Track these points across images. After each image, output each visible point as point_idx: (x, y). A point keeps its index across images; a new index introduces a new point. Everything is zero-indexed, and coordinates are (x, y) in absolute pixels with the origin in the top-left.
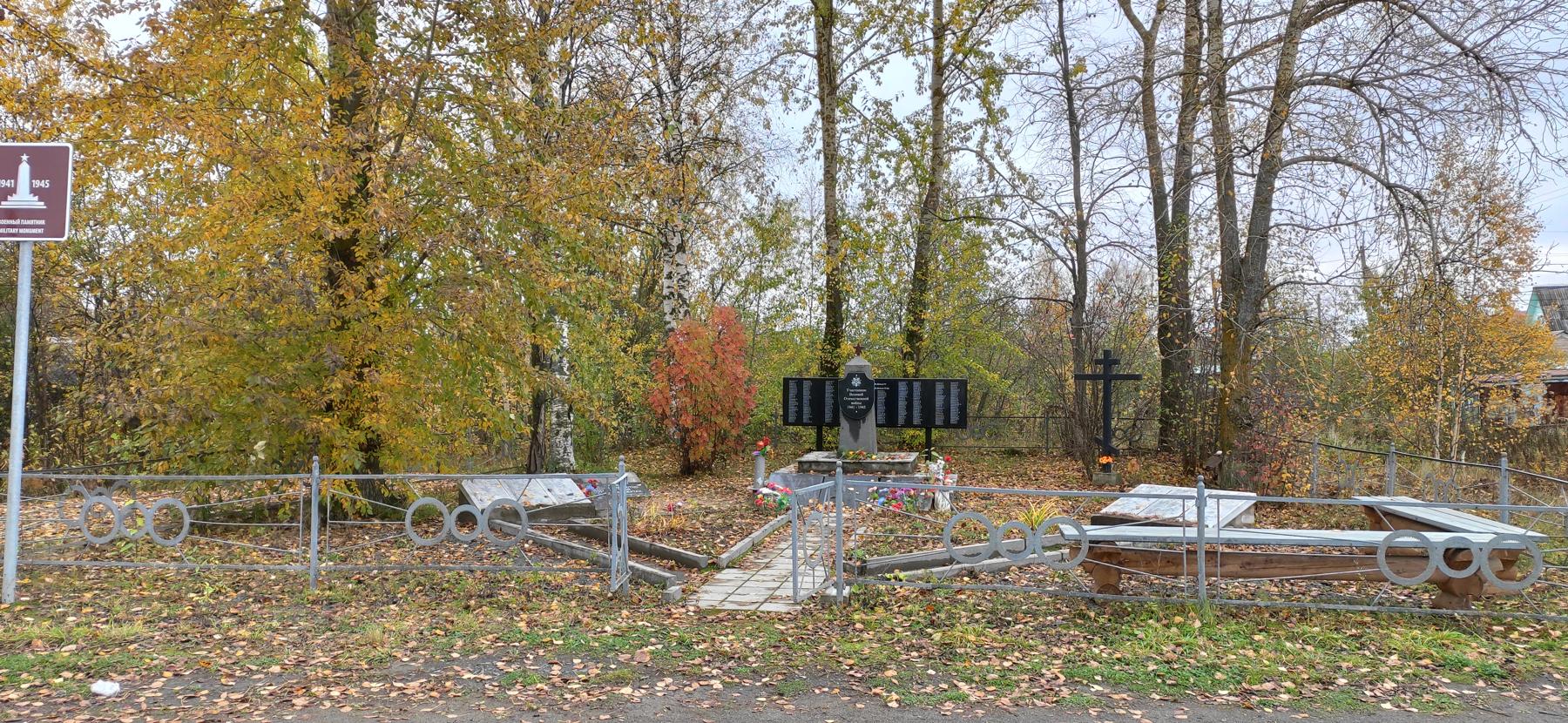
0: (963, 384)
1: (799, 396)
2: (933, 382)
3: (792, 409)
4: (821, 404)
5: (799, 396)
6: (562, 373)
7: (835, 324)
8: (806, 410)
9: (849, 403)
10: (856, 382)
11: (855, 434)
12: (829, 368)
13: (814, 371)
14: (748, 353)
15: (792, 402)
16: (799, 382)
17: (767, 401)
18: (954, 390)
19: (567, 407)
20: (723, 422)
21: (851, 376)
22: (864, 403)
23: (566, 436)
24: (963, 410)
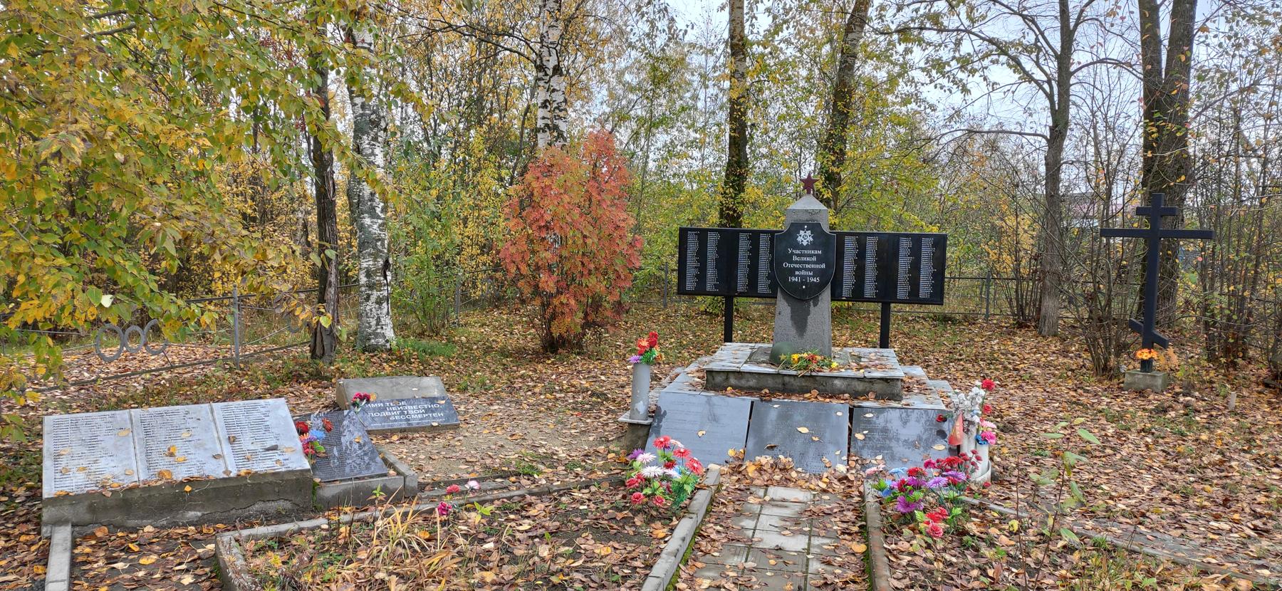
0: (940, 243)
1: (702, 254)
3: (691, 272)
4: (730, 266)
5: (702, 254)
6: (373, 215)
7: (738, 163)
8: (711, 273)
10: (805, 237)
11: (800, 323)
12: (731, 215)
14: (633, 197)
15: (692, 262)
16: (702, 234)
17: (660, 252)
18: (927, 251)
19: (381, 262)
20: (596, 284)
21: (796, 227)
23: (379, 302)
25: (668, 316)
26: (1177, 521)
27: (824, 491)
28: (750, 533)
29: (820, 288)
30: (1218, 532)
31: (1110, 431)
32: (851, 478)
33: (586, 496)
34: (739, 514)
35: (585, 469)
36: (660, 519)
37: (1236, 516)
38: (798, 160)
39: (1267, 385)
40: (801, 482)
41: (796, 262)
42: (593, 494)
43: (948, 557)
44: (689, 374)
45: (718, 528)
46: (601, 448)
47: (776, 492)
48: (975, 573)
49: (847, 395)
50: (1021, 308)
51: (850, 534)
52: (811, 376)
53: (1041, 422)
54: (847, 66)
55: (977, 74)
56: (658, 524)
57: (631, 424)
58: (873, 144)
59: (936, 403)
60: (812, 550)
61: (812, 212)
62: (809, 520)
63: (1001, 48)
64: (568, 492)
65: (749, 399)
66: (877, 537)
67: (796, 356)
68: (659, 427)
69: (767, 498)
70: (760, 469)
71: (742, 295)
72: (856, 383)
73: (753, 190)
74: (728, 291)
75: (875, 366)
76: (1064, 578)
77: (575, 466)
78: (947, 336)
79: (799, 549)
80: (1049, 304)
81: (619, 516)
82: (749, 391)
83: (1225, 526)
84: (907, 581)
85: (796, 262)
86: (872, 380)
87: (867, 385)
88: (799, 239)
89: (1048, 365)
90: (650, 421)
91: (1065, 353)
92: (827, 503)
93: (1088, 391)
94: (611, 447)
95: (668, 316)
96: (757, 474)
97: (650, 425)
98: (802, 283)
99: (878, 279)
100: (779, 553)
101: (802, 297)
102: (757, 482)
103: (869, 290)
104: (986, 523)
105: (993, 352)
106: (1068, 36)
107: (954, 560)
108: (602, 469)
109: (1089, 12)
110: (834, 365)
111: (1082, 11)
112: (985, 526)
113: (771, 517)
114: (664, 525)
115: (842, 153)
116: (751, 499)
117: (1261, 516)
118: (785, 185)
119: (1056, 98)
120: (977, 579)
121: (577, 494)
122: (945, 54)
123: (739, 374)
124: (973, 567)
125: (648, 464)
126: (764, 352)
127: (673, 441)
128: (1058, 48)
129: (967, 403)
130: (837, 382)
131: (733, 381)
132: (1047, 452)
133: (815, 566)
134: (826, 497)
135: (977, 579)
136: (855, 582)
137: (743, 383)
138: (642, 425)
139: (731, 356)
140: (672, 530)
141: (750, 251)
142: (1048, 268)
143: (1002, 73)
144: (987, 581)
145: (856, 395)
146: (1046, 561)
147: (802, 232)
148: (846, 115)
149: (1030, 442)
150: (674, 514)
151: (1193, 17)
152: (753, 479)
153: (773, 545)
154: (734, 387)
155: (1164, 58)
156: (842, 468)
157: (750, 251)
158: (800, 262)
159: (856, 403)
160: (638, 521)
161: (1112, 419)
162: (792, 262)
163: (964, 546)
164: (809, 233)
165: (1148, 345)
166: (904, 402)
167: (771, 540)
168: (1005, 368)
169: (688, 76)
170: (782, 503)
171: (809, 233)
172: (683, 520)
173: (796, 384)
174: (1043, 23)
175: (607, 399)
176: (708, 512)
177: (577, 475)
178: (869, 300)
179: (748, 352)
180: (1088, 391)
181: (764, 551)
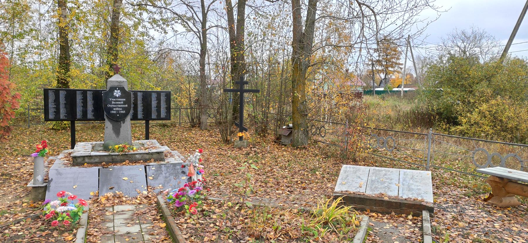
0: (168, 95)
1: (57, 101)
2: (75, 91)
3: (51, 111)
5: (57, 101)
7: (66, 58)
8: (63, 111)
9: (111, 109)
10: (117, 93)
12: (63, 83)
13: (55, 84)
18: (163, 98)
21: (113, 89)
22: (124, 109)
24: (168, 109)
25: (31, 132)
26: (267, 193)
27: (140, 204)
28: (112, 229)
29: (126, 115)
30: (279, 194)
31: (235, 164)
32: (150, 196)
33: (19, 228)
34: (104, 221)
35: (11, 214)
36: (67, 231)
37: (282, 188)
38: (90, 59)
39: (275, 142)
40: (128, 202)
41: (114, 104)
42: (23, 225)
43: (201, 221)
44: (60, 159)
45: (96, 230)
46: (18, 202)
47: (118, 208)
48: (212, 225)
49: (142, 161)
50: (193, 120)
51: (157, 220)
52: (125, 154)
53: (212, 163)
54: (115, 17)
55: (169, 27)
56: (66, 234)
57: (34, 187)
58: (128, 52)
59: (180, 161)
60: (143, 230)
61: (120, 82)
62: (136, 217)
63: (180, 17)
64: (8, 227)
65: (97, 168)
66: (171, 219)
67: (117, 146)
68: (49, 186)
69: (115, 211)
70: (108, 199)
71: (79, 120)
72: (145, 155)
73: (73, 71)
74: (72, 117)
75: (152, 147)
76: (242, 221)
77: (4, 213)
78: (167, 133)
79: (137, 231)
80: (203, 118)
81: (44, 234)
82: (96, 164)
83: (281, 192)
84: (189, 235)
85: (114, 104)
86: (152, 154)
87: (150, 156)
88: (115, 94)
89: (206, 141)
90: (44, 185)
91: (211, 136)
92: (143, 208)
93: (223, 150)
94: (24, 200)
95: (31, 132)
96: (106, 202)
97: (46, 186)
98: (117, 114)
99: (143, 110)
100: (129, 235)
101: (117, 120)
102: (107, 205)
103: (140, 116)
104: (209, 205)
105: (186, 138)
106: (205, 15)
107: (203, 222)
108: (21, 212)
109: (211, 7)
110: (135, 149)
111: (209, 6)
112: (209, 206)
113: (119, 220)
114: (70, 234)
115: (116, 55)
116: (107, 213)
117: (289, 187)
118: (87, 70)
119: (202, 39)
120: (213, 227)
121: (14, 228)
122: (157, 17)
123: (90, 157)
124: (210, 223)
125: (54, 205)
126: (99, 145)
127: (67, 193)
128: (201, 19)
129: (194, 159)
130: (137, 156)
131: (87, 160)
132: (218, 174)
133: (147, 237)
134: (141, 206)
135: (213, 227)
136: (166, 240)
137: (92, 160)
138: (41, 187)
139: (82, 148)
140: (75, 235)
141: (83, 99)
142: (201, 104)
143: (179, 27)
144: (217, 227)
145: (146, 161)
146: (234, 215)
147: (116, 91)
148: (117, 39)
149: (211, 171)
150: (74, 228)
151: (244, 13)
152: (105, 204)
153: (125, 232)
154: (88, 163)
155: (235, 27)
156: (145, 193)
157: (83, 99)
158: (116, 104)
159: (147, 164)
160: (55, 234)
161: (234, 159)
162: (111, 104)
163: (204, 215)
164: (119, 91)
165: (241, 131)
166: (166, 161)
167: (123, 230)
168: (192, 143)
169: (30, 14)
170: (122, 212)
171: (119, 91)
172: (79, 230)
173: (119, 158)
174: (196, 9)
175: (12, 176)
176: (88, 223)
177: (7, 217)
178: (140, 120)
179: (91, 146)
180: (223, 150)
181: (121, 235)
